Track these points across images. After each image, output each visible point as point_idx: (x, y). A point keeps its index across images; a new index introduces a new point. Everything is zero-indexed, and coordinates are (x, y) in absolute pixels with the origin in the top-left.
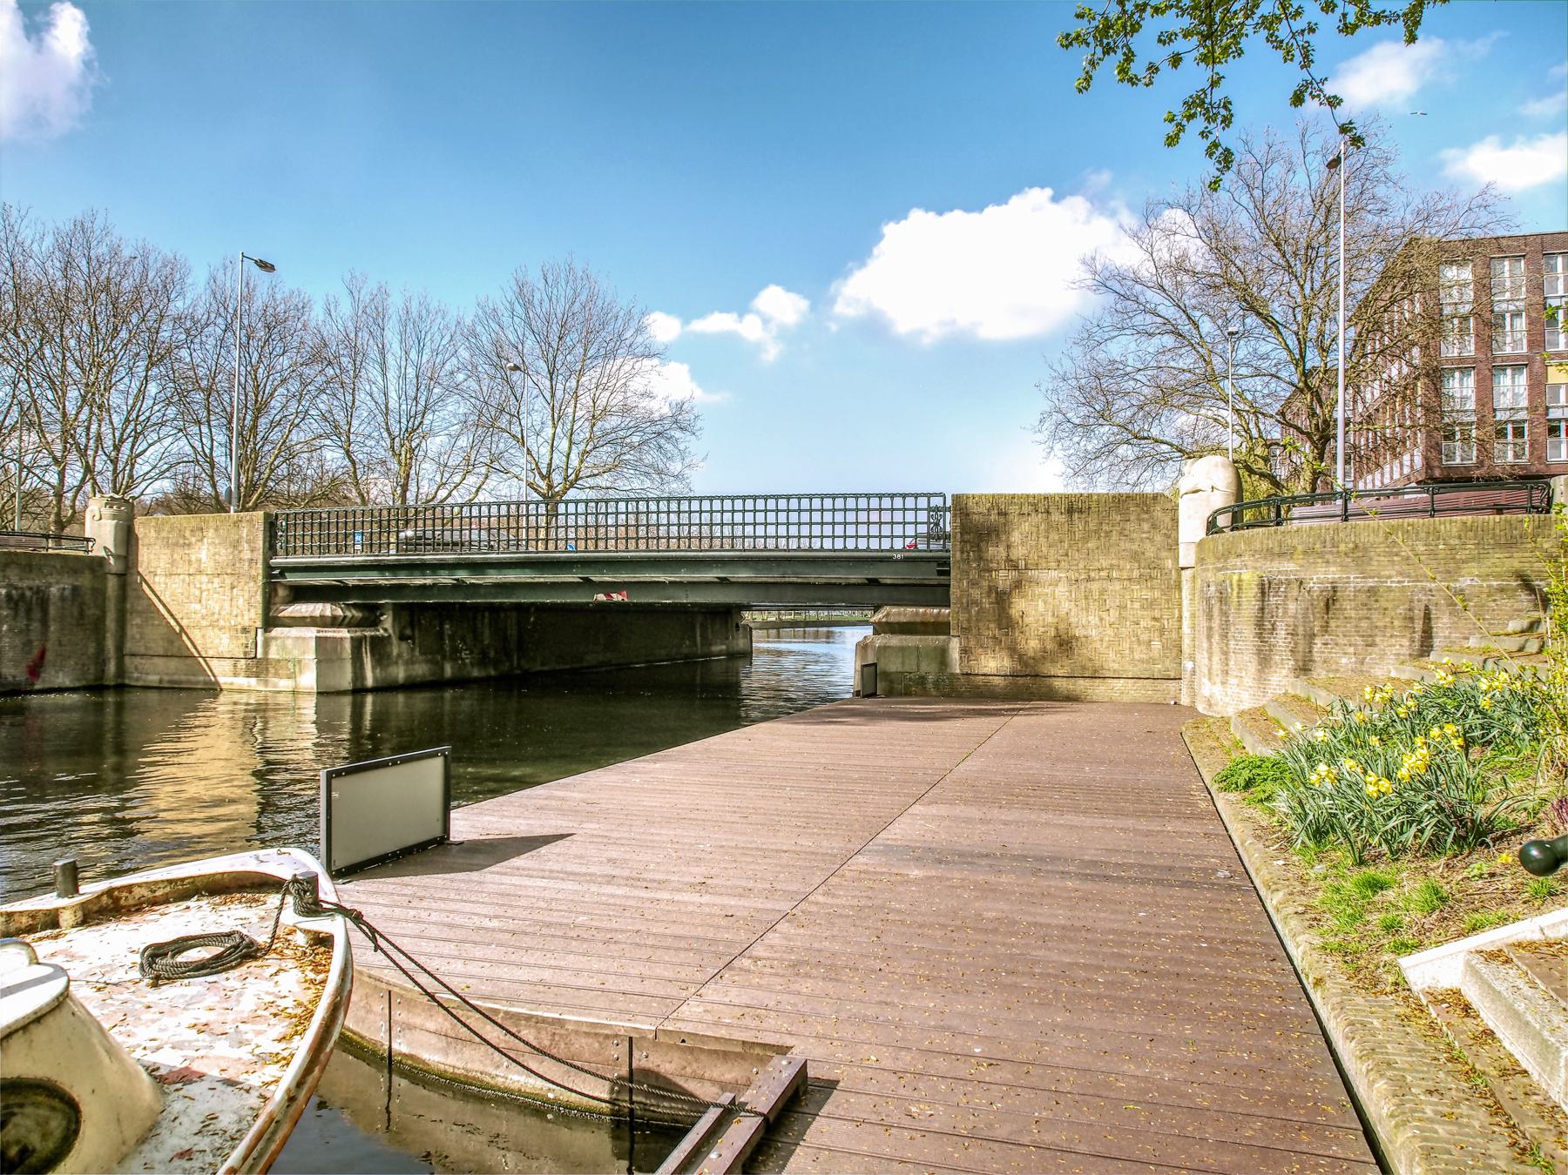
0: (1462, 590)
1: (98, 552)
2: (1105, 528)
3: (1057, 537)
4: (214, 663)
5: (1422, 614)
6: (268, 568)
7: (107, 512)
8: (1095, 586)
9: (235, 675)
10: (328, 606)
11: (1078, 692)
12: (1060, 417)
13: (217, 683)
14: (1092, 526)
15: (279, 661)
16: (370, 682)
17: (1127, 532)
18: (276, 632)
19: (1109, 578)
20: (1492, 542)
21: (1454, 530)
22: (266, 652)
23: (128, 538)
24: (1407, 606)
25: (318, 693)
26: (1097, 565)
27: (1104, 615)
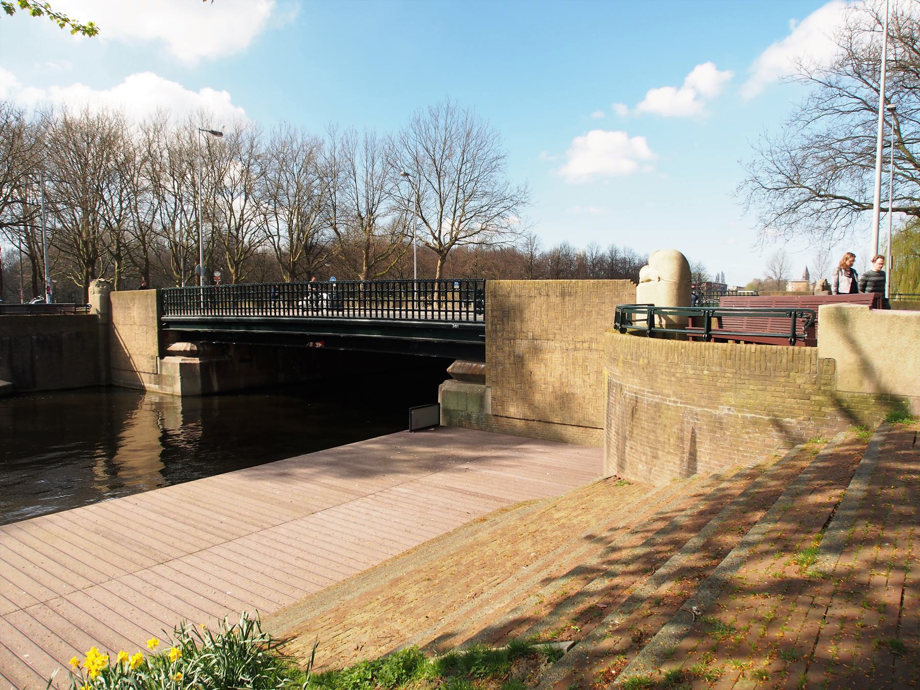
0: (720, 418)
1: (92, 312)
2: (587, 308)
3: (553, 315)
4: (142, 375)
5: (690, 437)
6: (160, 322)
7: (97, 289)
8: (579, 354)
9: (151, 383)
10: (190, 344)
11: (568, 436)
12: (756, 184)
13: (144, 387)
14: (578, 307)
15: (166, 376)
16: (216, 388)
17: (602, 312)
18: (167, 359)
19: (590, 349)
20: (747, 372)
21: (716, 356)
22: (161, 371)
23: (107, 304)
24: (679, 426)
25: (182, 396)
26: (581, 338)
27: (586, 378)
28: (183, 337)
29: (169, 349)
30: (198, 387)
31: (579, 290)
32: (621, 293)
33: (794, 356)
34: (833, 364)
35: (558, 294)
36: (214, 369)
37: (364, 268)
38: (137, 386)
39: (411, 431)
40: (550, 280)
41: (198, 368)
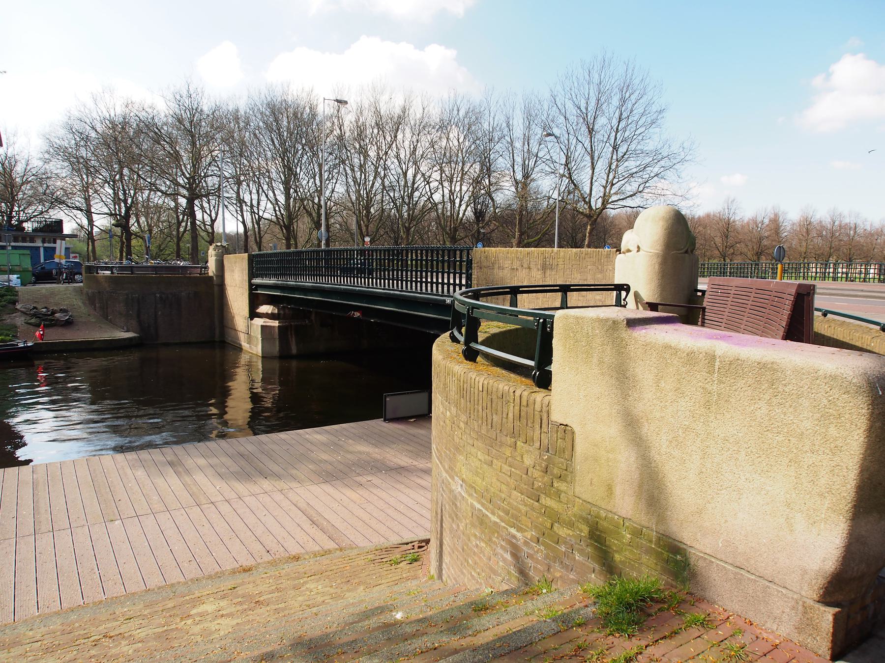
1: (211, 274)
6: (251, 285)
13: (241, 345)
16: (294, 351)
28: (271, 300)
29: (258, 311)
30: (276, 349)
31: (561, 262)
32: (605, 267)
33: (522, 408)
34: (570, 437)
35: (539, 267)
36: (293, 333)
37: (517, 234)
38: (237, 344)
39: (385, 420)
40: (533, 249)
41: (277, 330)
